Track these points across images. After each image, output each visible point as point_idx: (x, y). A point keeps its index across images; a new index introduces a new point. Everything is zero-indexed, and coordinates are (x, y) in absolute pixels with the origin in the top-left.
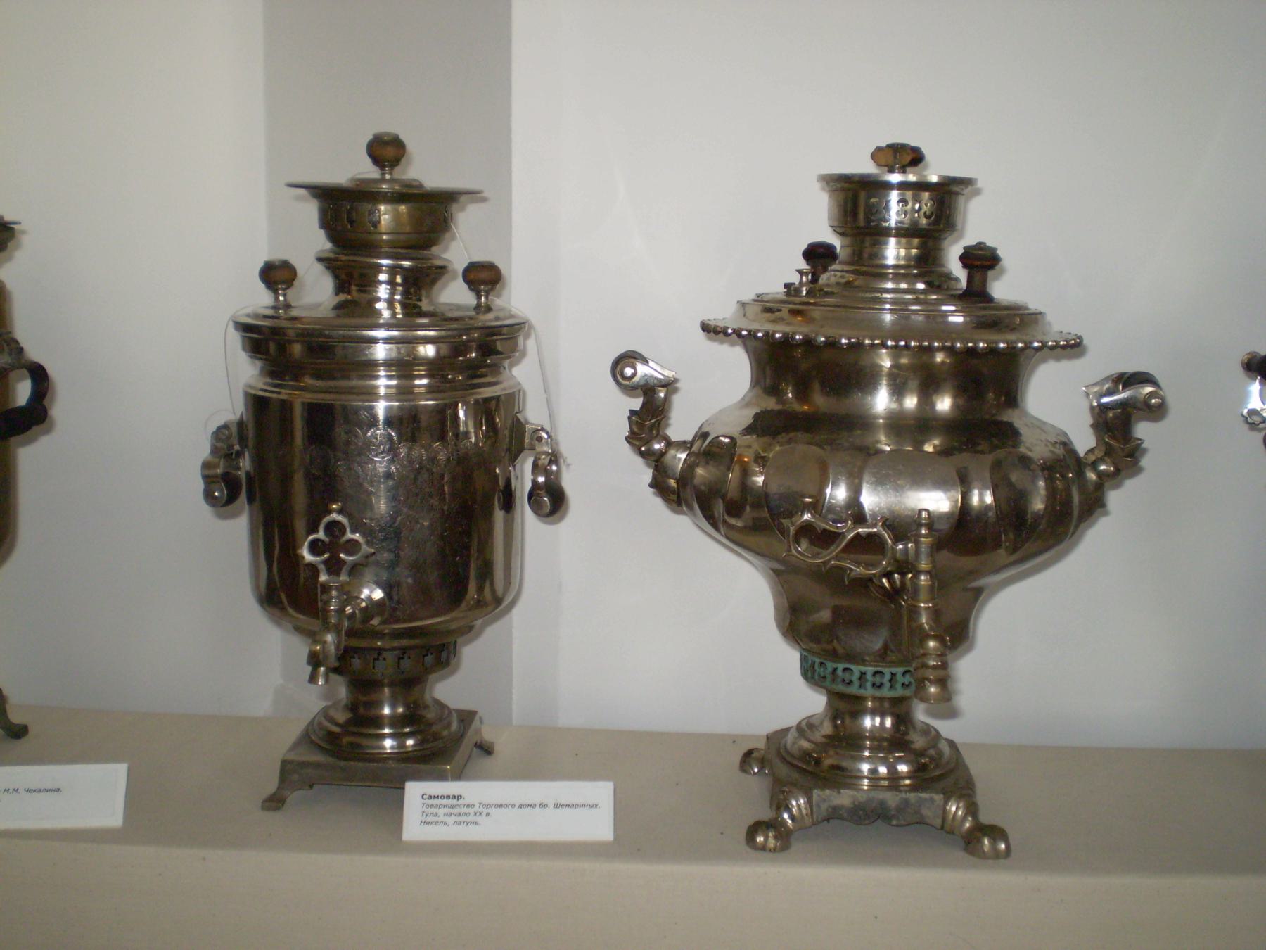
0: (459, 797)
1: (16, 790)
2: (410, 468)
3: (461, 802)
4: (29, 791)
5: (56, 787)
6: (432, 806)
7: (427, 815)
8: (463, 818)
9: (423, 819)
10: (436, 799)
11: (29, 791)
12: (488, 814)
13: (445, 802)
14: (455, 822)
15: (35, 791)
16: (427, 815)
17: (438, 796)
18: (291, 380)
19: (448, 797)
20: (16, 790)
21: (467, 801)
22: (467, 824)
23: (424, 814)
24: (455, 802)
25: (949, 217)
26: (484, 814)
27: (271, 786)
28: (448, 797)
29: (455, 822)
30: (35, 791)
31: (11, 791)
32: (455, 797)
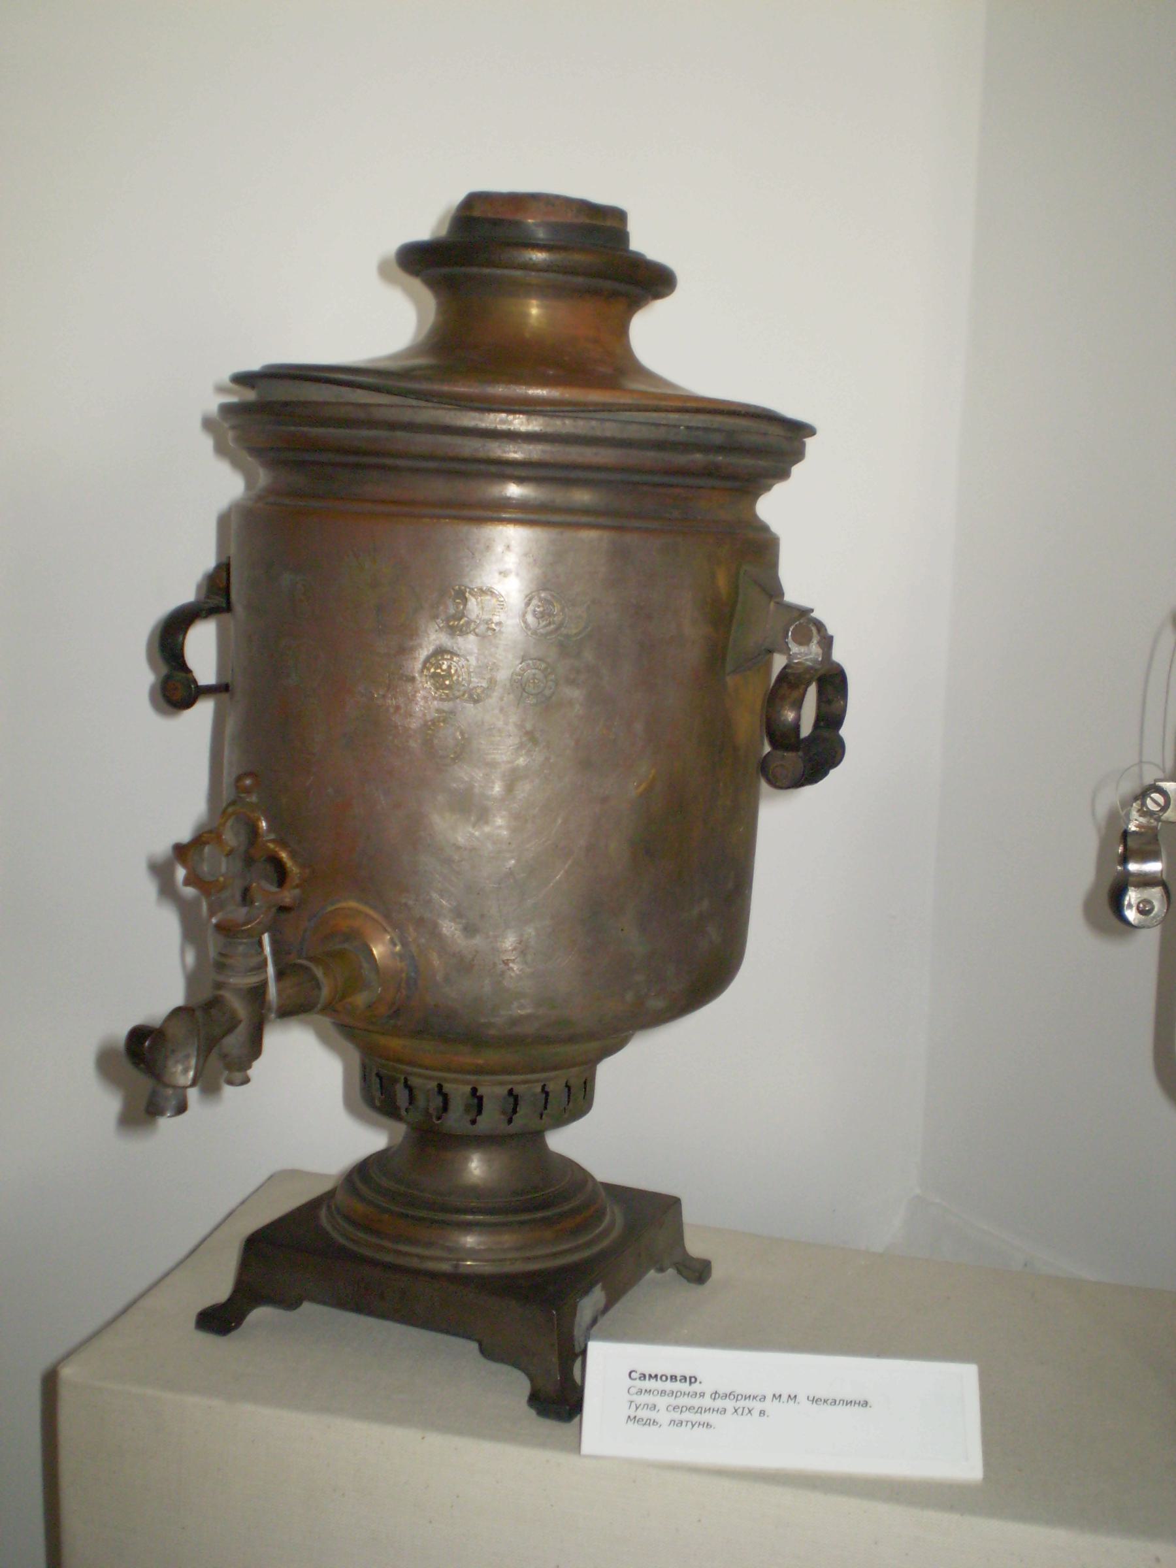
0: (692, 1380)
1: (793, 1398)
2: (565, 625)
3: (696, 1387)
4: (815, 1400)
5: (861, 1398)
6: (649, 1392)
7: (637, 1408)
8: (687, 1416)
9: (632, 1413)
10: (653, 1381)
11: (815, 1400)
12: (762, 1413)
13: (669, 1386)
14: (672, 1422)
15: (825, 1401)
16: (637, 1408)
17: (656, 1376)
18: (798, 705)
19: (673, 1378)
20: (793, 1398)
21: (707, 1387)
22: (693, 1426)
23: (633, 1406)
24: (685, 1387)
25: (548, 266)
26: (756, 1413)
27: (220, 1289)
28: (673, 1378)
29: (672, 1422)
30: (825, 1401)
31: (784, 1398)
32: (685, 1378)
